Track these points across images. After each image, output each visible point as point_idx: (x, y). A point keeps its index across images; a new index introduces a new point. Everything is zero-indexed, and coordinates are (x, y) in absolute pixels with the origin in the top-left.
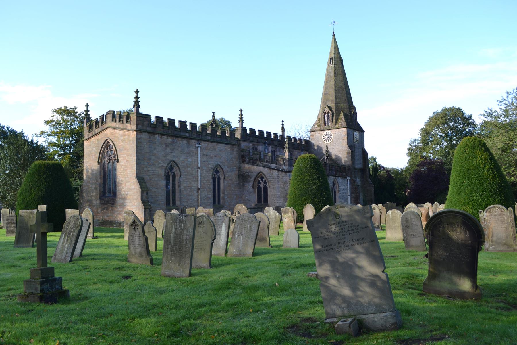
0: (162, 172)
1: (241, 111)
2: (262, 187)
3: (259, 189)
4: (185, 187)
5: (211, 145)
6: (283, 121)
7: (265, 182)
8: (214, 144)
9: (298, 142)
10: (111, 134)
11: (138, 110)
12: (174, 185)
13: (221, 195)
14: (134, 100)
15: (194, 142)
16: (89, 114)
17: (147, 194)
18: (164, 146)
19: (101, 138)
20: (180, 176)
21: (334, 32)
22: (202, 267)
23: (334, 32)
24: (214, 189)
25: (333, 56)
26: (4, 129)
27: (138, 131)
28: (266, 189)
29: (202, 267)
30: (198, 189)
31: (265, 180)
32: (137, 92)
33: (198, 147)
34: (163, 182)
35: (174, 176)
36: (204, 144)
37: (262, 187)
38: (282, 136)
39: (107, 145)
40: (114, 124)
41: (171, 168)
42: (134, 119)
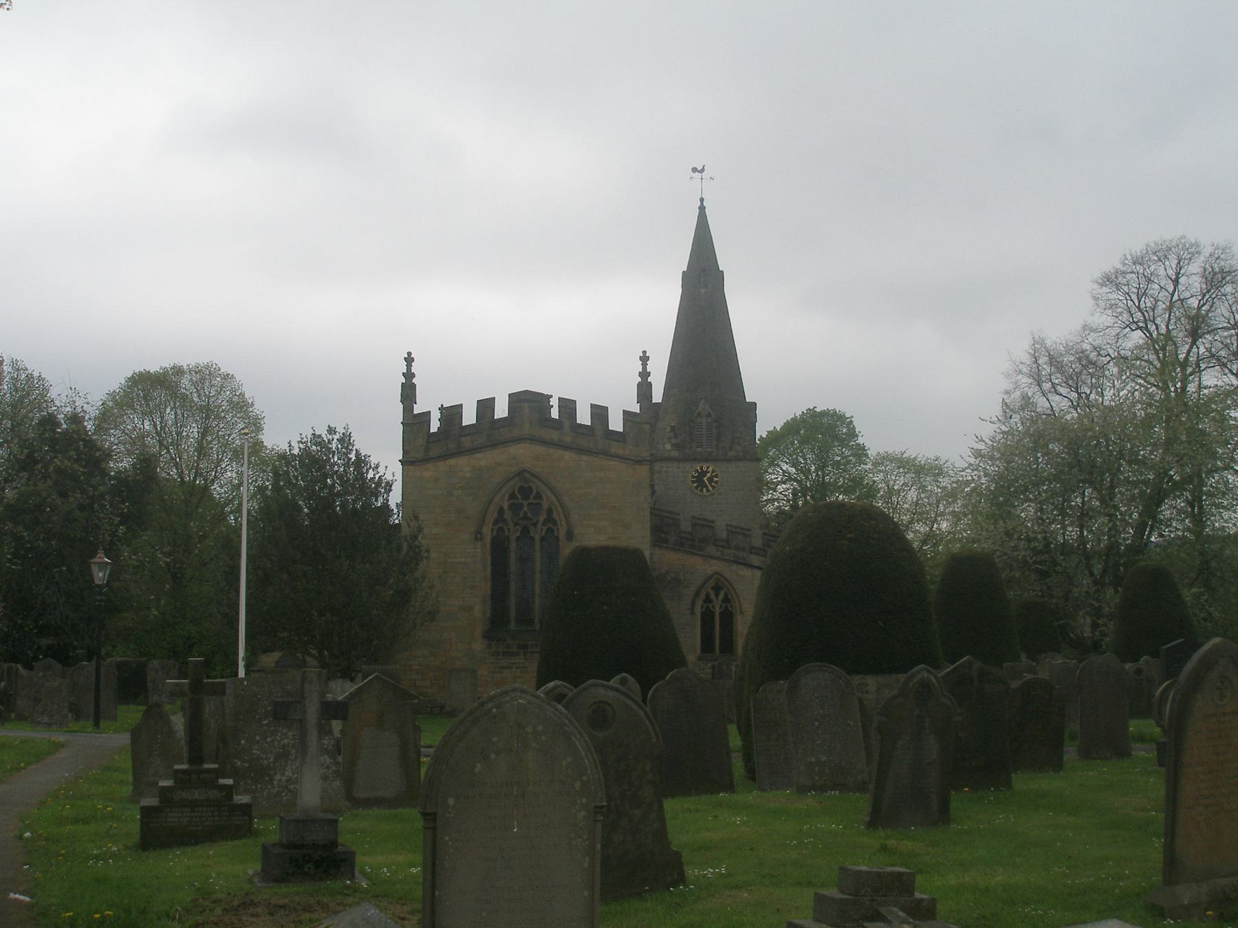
2: (718, 611)
3: (707, 617)
7: (727, 600)
21: (702, 200)
23: (702, 200)
26: (435, 426)
31: (726, 595)
37: (718, 611)
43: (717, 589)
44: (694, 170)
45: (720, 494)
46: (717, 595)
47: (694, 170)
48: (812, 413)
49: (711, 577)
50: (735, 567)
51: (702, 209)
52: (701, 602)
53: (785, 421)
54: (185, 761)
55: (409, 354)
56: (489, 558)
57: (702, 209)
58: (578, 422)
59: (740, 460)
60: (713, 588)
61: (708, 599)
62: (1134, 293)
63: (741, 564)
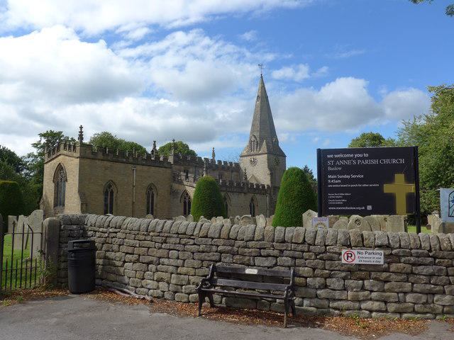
0: (101, 189)
3: (185, 203)
4: (121, 201)
5: (146, 168)
8: (148, 167)
9: (229, 165)
10: (63, 159)
11: (81, 142)
12: (112, 199)
13: (155, 208)
15: (130, 166)
16: (323, 156)
18: (104, 169)
19: (55, 163)
22: (129, 32)
24: (148, 203)
25: (260, 94)
27: (81, 157)
29: (129, 32)
30: (133, 203)
34: (102, 197)
35: (112, 193)
36: (139, 167)
38: (213, 161)
39: (60, 168)
40: (65, 152)
41: (110, 186)
42: (78, 148)
58: (385, 192)
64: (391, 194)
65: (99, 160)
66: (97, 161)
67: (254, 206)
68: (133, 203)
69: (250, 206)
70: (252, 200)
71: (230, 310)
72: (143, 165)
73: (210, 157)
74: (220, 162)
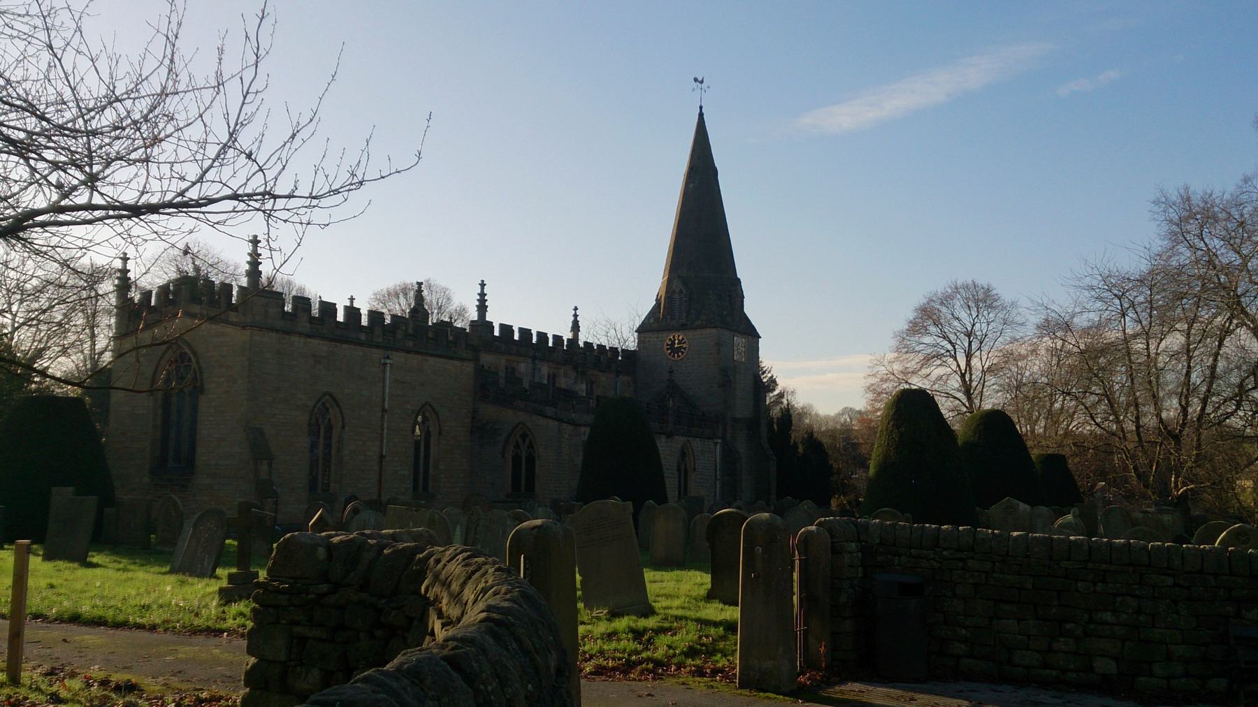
1: (483, 285)
2: (524, 455)
3: (516, 459)
5: (414, 360)
6: (576, 309)
7: (531, 446)
8: (420, 357)
12: (328, 446)
14: (249, 259)
15: (377, 354)
17: (270, 465)
20: (343, 427)
21: (701, 108)
23: (701, 108)
28: (531, 460)
32: (483, 285)
33: (385, 364)
35: (329, 429)
36: (398, 357)
37: (524, 455)
38: (573, 341)
43: (524, 436)
44: (696, 80)
45: (688, 359)
46: (524, 442)
47: (696, 80)
48: (740, 279)
49: (516, 427)
50: (534, 417)
51: (701, 115)
52: (512, 448)
53: (476, 309)
54: (171, 550)
55: (483, 281)
56: (160, 411)
57: (701, 115)
58: (487, 319)
59: (704, 328)
60: (521, 436)
61: (517, 446)
62: (311, 201)
63: (540, 415)
64: (666, 498)
65: (300, 334)
66: (295, 339)
67: (686, 470)
68: (382, 457)
69: (679, 470)
70: (683, 454)
71: (1165, 335)
72: (408, 352)
73: (567, 335)
74: (506, 329)
